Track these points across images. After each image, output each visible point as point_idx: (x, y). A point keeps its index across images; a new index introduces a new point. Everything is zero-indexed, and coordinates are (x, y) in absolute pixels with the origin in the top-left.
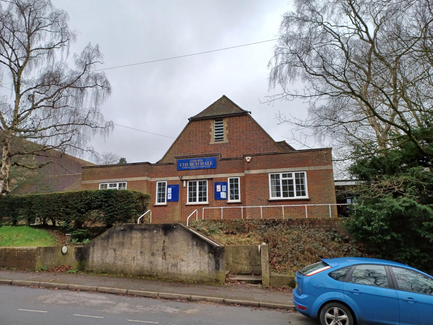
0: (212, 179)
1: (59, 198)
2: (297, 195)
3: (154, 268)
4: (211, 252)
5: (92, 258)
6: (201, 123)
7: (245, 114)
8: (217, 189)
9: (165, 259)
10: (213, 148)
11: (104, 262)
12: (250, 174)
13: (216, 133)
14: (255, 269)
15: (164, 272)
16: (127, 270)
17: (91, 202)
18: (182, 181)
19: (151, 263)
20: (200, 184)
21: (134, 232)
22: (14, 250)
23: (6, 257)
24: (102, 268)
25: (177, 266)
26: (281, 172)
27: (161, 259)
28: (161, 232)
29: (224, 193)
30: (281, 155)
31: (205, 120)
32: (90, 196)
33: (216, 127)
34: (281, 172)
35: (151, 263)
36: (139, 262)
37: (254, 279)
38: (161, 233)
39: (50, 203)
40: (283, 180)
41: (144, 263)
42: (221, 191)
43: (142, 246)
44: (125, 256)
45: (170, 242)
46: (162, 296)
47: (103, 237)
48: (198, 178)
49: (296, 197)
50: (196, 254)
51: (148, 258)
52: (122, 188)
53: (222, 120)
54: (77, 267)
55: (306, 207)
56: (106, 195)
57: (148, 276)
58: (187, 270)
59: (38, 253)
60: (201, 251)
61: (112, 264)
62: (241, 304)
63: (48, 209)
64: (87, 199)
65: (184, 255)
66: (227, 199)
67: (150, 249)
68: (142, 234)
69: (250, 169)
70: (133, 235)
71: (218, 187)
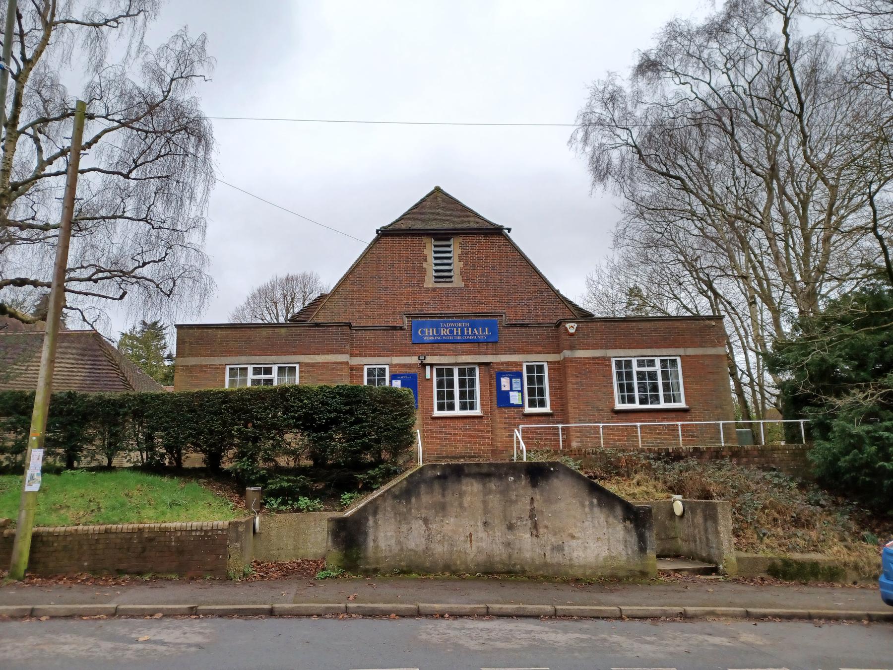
0: (487, 364)
1: (224, 402)
2: (666, 401)
3: (515, 555)
4: (629, 519)
5: (374, 541)
6: (402, 242)
7: (497, 232)
8: (502, 384)
9: (537, 536)
10: (431, 295)
11: (405, 548)
12: (575, 358)
13: (436, 265)
14: (668, 546)
15: (537, 563)
16: (458, 562)
17: (313, 414)
18: (424, 366)
19: (508, 544)
20: (462, 373)
21: (465, 481)
22: (165, 531)
23: (144, 550)
24: (401, 561)
25: (563, 550)
26: (635, 357)
27: (528, 535)
28: (524, 481)
29: (516, 393)
30: (634, 324)
31: (413, 235)
32: (308, 398)
33: (436, 252)
34: (634, 357)
35: (508, 544)
36: (483, 545)
37: (703, 567)
38: (523, 483)
39: (199, 415)
40: (638, 373)
41: (494, 546)
42: (511, 390)
43: (486, 511)
44: (450, 534)
45: (545, 501)
46: (629, 613)
47: (397, 493)
48: (460, 361)
49: (663, 405)
50: (599, 524)
51: (500, 534)
52: (286, 381)
53: (448, 240)
54: (340, 564)
55: (802, 425)
56: (348, 396)
57: (503, 573)
58: (583, 556)
59: (233, 535)
60: (609, 516)
61: (424, 551)
62: (781, 617)
63: (194, 429)
64: (302, 407)
65: (576, 527)
66: (522, 406)
67: (505, 517)
68: (484, 485)
69: (574, 347)
70: (464, 488)
71: (505, 382)
